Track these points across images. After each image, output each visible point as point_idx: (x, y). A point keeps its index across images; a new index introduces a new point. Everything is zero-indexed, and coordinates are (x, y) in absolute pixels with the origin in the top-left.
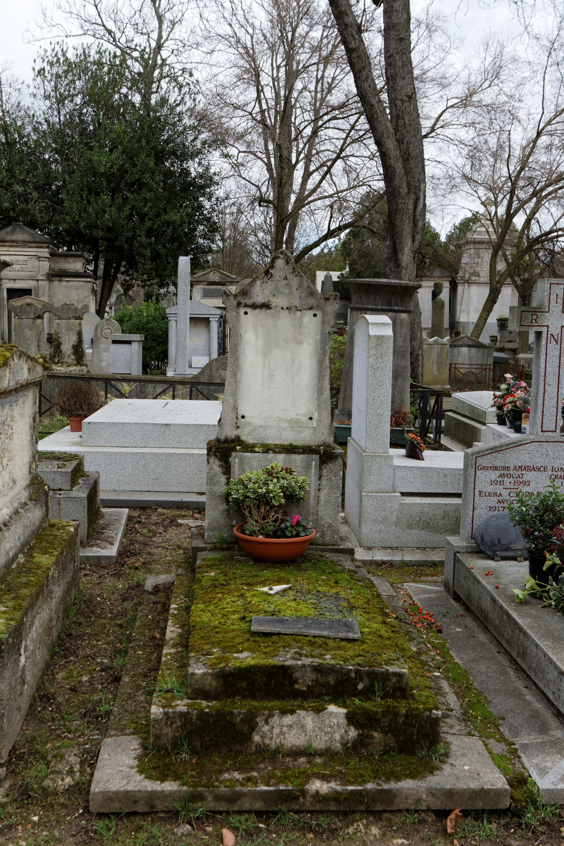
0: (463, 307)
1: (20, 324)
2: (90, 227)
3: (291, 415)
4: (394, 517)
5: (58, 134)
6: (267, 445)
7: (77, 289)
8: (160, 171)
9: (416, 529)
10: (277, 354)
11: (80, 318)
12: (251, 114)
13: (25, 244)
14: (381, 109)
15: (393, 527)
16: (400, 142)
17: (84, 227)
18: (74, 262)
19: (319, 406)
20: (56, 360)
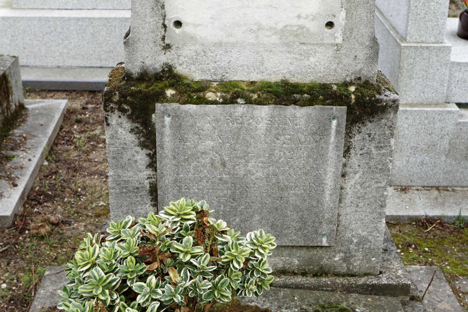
3: (286, 18)
15: (443, 158)
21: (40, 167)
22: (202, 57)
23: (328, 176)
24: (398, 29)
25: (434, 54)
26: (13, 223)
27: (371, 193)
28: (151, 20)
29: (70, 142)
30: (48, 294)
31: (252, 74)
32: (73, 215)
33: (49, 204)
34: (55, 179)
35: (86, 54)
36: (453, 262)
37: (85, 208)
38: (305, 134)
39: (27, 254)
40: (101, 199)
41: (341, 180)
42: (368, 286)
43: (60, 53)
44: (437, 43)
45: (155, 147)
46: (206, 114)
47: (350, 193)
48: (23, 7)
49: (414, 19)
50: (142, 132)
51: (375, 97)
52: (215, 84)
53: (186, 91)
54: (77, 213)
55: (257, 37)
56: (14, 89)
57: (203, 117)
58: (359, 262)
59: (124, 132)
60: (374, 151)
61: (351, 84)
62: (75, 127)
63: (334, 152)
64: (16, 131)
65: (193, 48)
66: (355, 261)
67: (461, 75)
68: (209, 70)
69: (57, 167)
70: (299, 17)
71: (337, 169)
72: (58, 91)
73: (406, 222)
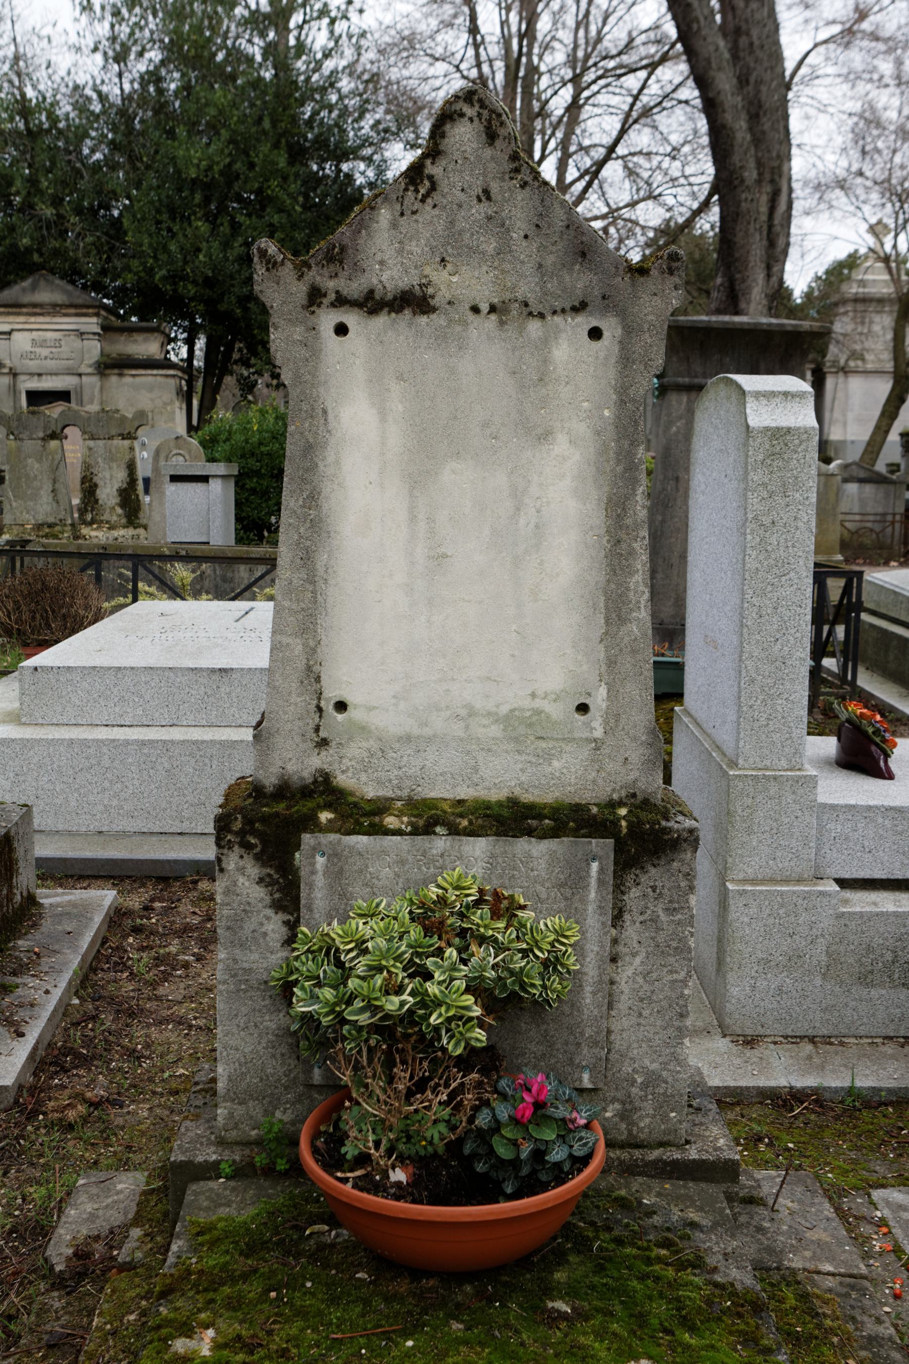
0: (837, 414)
1: (19, 450)
2: (175, 277)
3: (513, 697)
4: (819, 953)
5: (122, 115)
6: (429, 804)
7: (151, 389)
8: (297, 175)
9: (882, 985)
10: (458, 479)
11: (130, 436)
12: (457, 67)
13: (55, 309)
14: (706, 12)
15: (818, 981)
16: (743, 81)
17: (164, 278)
18: (146, 340)
19: (611, 663)
20: (89, 517)
21: (64, 1009)
22: (378, 759)
23: (588, 960)
24: (724, 748)
25: (787, 789)
26: (16, 1102)
27: (662, 991)
28: (299, 699)
29: (121, 965)
30: (84, 1216)
31: (459, 789)
32: (127, 1090)
33: (82, 1072)
34: (92, 1030)
35: (155, 809)
36: (839, 1167)
37: (151, 1080)
38: (547, 885)
39: (41, 1156)
40: (180, 1064)
41: (609, 968)
42: (665, 1163)
43: (105, 806)
44: (791, 770)
45: (298, 909)
46: (385, 852)
47: (626, 991)
48: (40, 721)
49: (749, 728)
50: (278, 882)
51: (659, 824)
52: (399, 804)
53: (352, 813)
54: (135, 1087)
55: (467, 727)
56: (21, 864)
57: (378, 857)
58: (647, 1120)
59: (247, 884)
60: (663, 917)
61: (621, 803)
62: (131, 940)
63: (597, 916)
64: (20, 942)
65: (364, 744)
66: (641, 1118)
67: (839, 827)
68: (390, 781)
69: (97, 1009)
70: (533, 695)
71: (602, 947)
72: (96, 877)
73: (754, 1100)
